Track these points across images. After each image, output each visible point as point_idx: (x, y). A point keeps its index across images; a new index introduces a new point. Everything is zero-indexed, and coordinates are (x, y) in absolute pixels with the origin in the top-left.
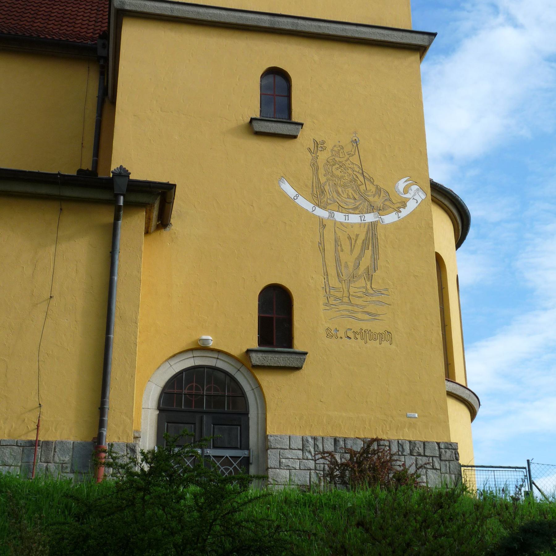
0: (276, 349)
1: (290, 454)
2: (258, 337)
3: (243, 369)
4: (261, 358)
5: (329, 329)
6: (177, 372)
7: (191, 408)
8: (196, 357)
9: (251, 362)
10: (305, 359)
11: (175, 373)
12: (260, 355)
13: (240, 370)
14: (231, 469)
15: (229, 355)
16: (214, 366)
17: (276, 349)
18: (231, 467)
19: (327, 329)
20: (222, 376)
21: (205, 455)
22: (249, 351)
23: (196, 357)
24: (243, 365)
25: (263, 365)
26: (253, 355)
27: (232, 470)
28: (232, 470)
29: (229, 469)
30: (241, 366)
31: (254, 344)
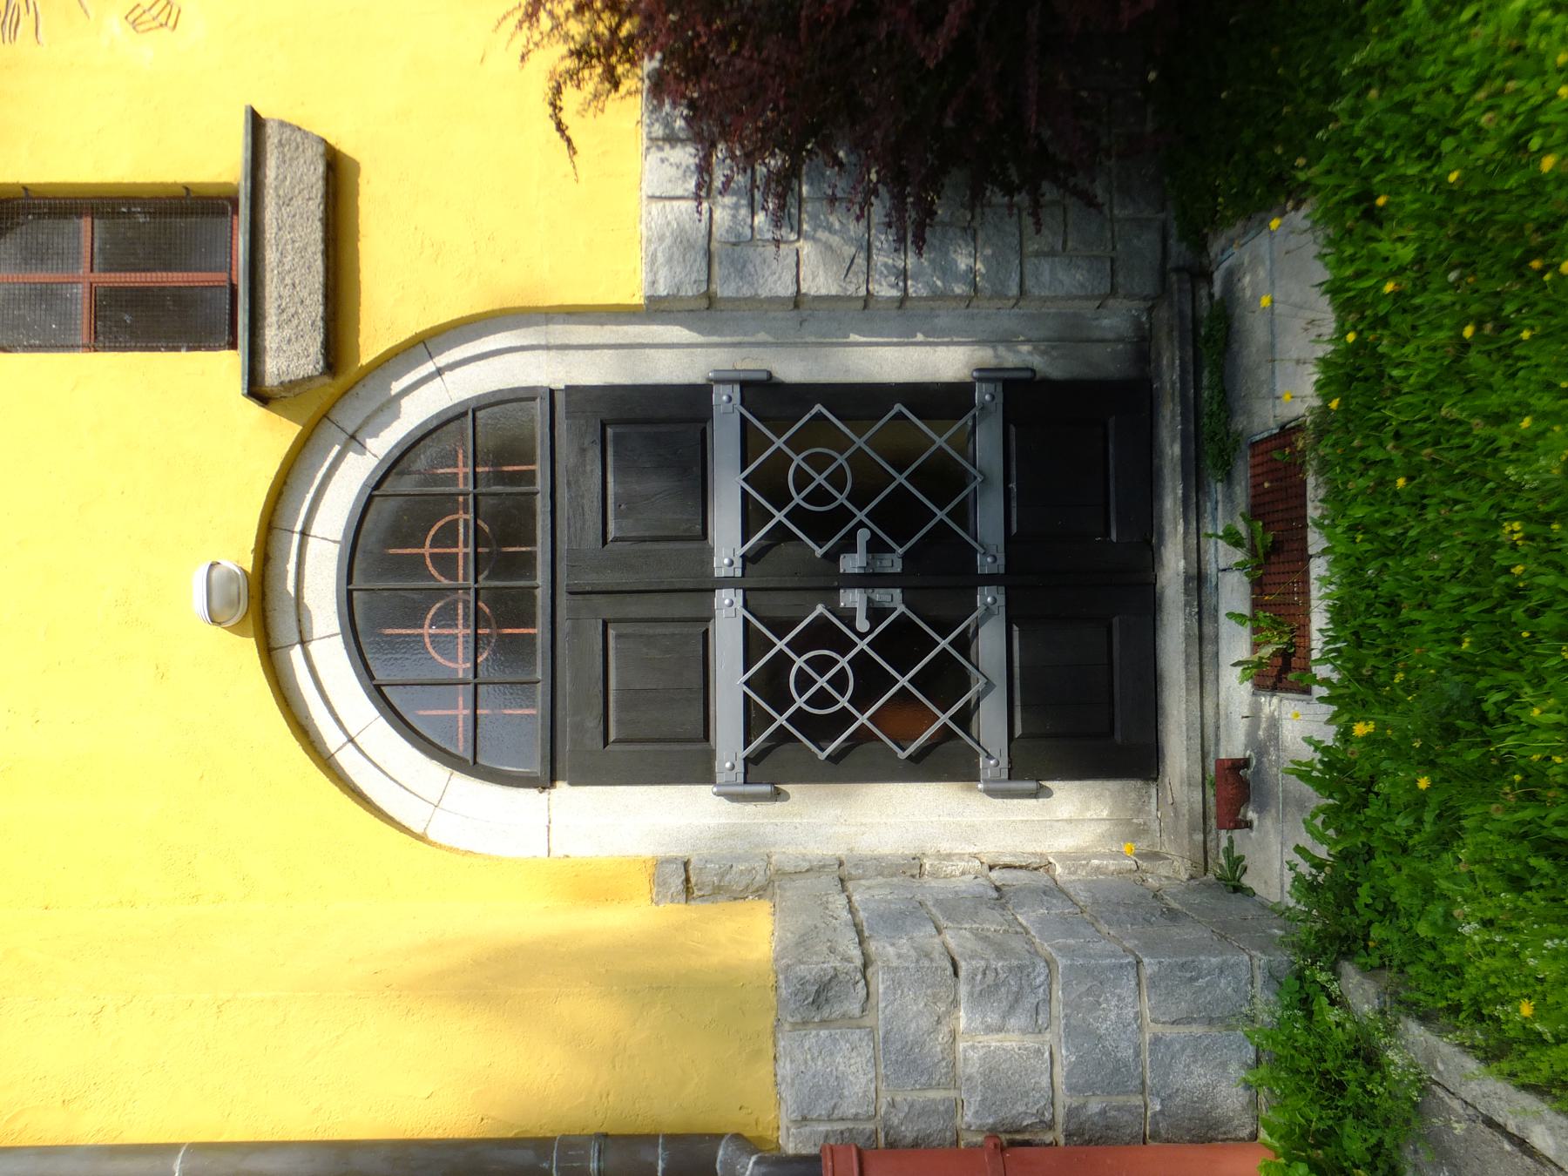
0: (1014, 504)
1: (973, 986)
2: (190, 349)
3: (349, 418)
4: (287, 332)
5: (131, 18)
6: (376, 713)
7: (539, 641)
8: (300, 632)
9: (310, 378)
10: (282, 124)
11: (382, 718)
12: (272, 336)
13: (350, 431)
14: (844, 702)
15: (285, 483)
16: (338, 546)
17: (1014, 504)
18: (841, 453)
19: (134, 24)
20: (384, 510)
21: (739, 573)
22: (256, 390)
23: (300, 632)
24: (325, 416)
25: (320, 324)
26: (274, 369)
27: (428, 542)
28: (428, 542)
29: (804, 499)
30: (329, 424)
31: (227, 365)
